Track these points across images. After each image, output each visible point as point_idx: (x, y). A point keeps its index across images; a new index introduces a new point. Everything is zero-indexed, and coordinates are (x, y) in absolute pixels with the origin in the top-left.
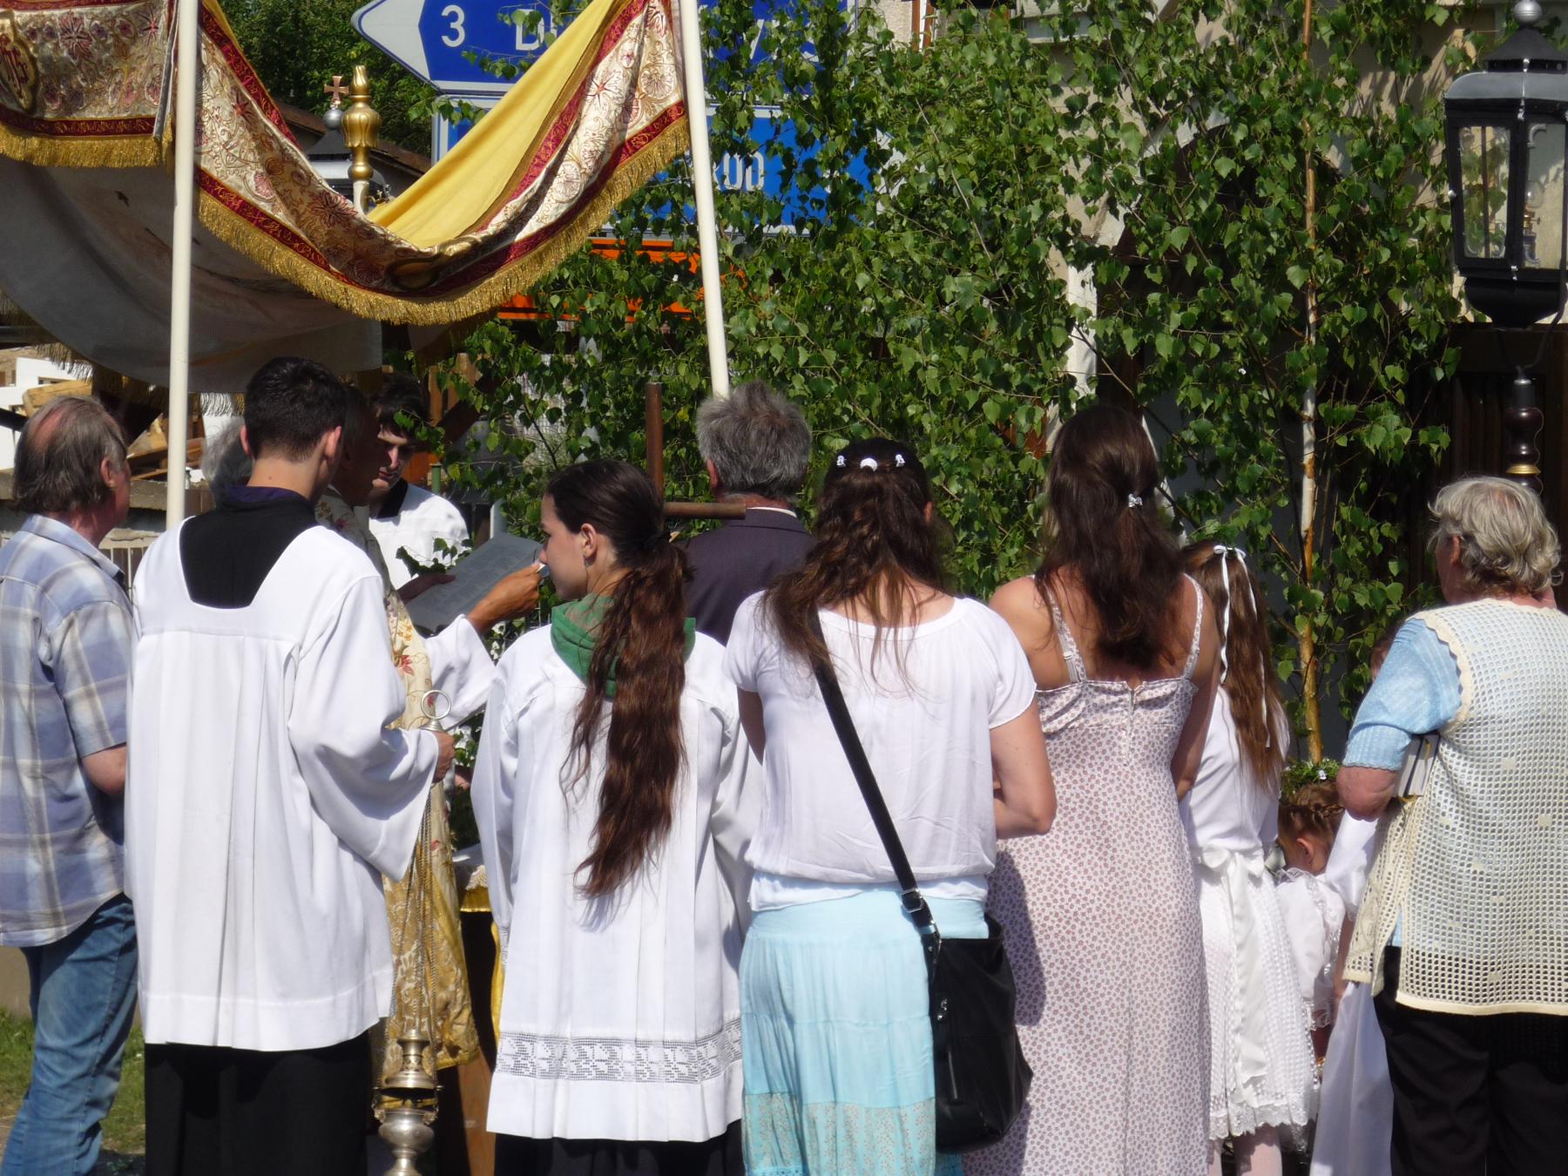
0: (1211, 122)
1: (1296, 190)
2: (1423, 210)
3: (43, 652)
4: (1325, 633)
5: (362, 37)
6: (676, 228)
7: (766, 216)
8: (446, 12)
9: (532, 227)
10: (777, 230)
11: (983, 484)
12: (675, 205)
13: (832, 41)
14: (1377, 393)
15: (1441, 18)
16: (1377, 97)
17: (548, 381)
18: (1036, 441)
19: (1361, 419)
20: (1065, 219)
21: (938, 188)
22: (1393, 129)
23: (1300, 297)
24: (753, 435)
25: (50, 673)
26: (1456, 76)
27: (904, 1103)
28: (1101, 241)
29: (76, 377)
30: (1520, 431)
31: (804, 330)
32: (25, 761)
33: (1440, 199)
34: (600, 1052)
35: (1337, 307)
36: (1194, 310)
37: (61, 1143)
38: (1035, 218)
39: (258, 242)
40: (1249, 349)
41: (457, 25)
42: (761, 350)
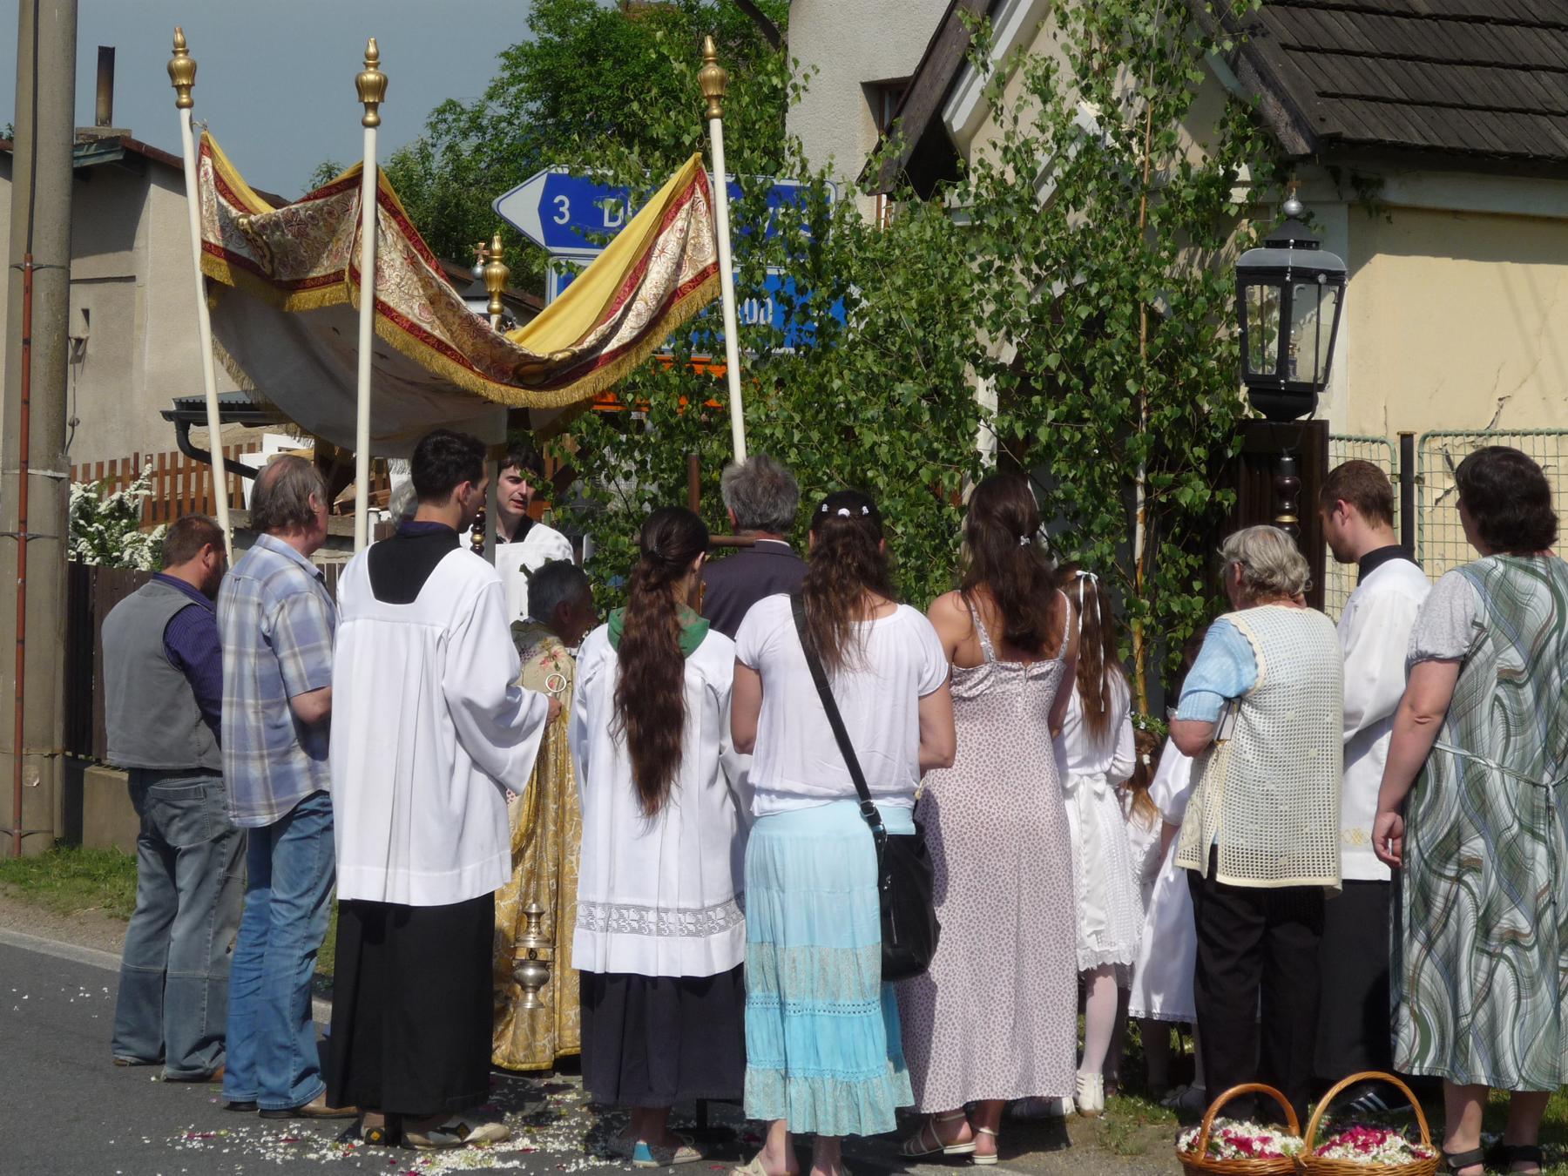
0: (1079, 279)
1: (1134, 327)
2: (1220, 342)
3: (264, 627)
4: (1150, 629)
5: (503, 219)
6: (712, 349)
7: (773, 342)
8: (557, 200)
9: (614, 344)
10: (781, 351)
11: (919, 526)
12: (711, 333)
13: (820, 224)
14: (1187, 466)
15: (1233, 212)
16: (1190, 264)
17: (626, 451)
18: (956, 496)
19: (1177, 483)
20: (976, 344)
21: (892, 325)
22: (1199, 287)
23: (1136, 401)
24: (760, 490)
25: (269, 640)
26: (1243, 252)
27: (859, 945)
28: (1001, 360)
29: (303, 447)
30: (1284, 493)
31: (797, 418)
32: (250, 701)
33: (1231, 334)
34: (633, 915)
35: (1161, 407)
36: (1063, 408)
37: (286, 963)
38: (956, 345)
39: (423, 352)
40: (1101, 435)
41: (564, 209)
42: (768, 431)
